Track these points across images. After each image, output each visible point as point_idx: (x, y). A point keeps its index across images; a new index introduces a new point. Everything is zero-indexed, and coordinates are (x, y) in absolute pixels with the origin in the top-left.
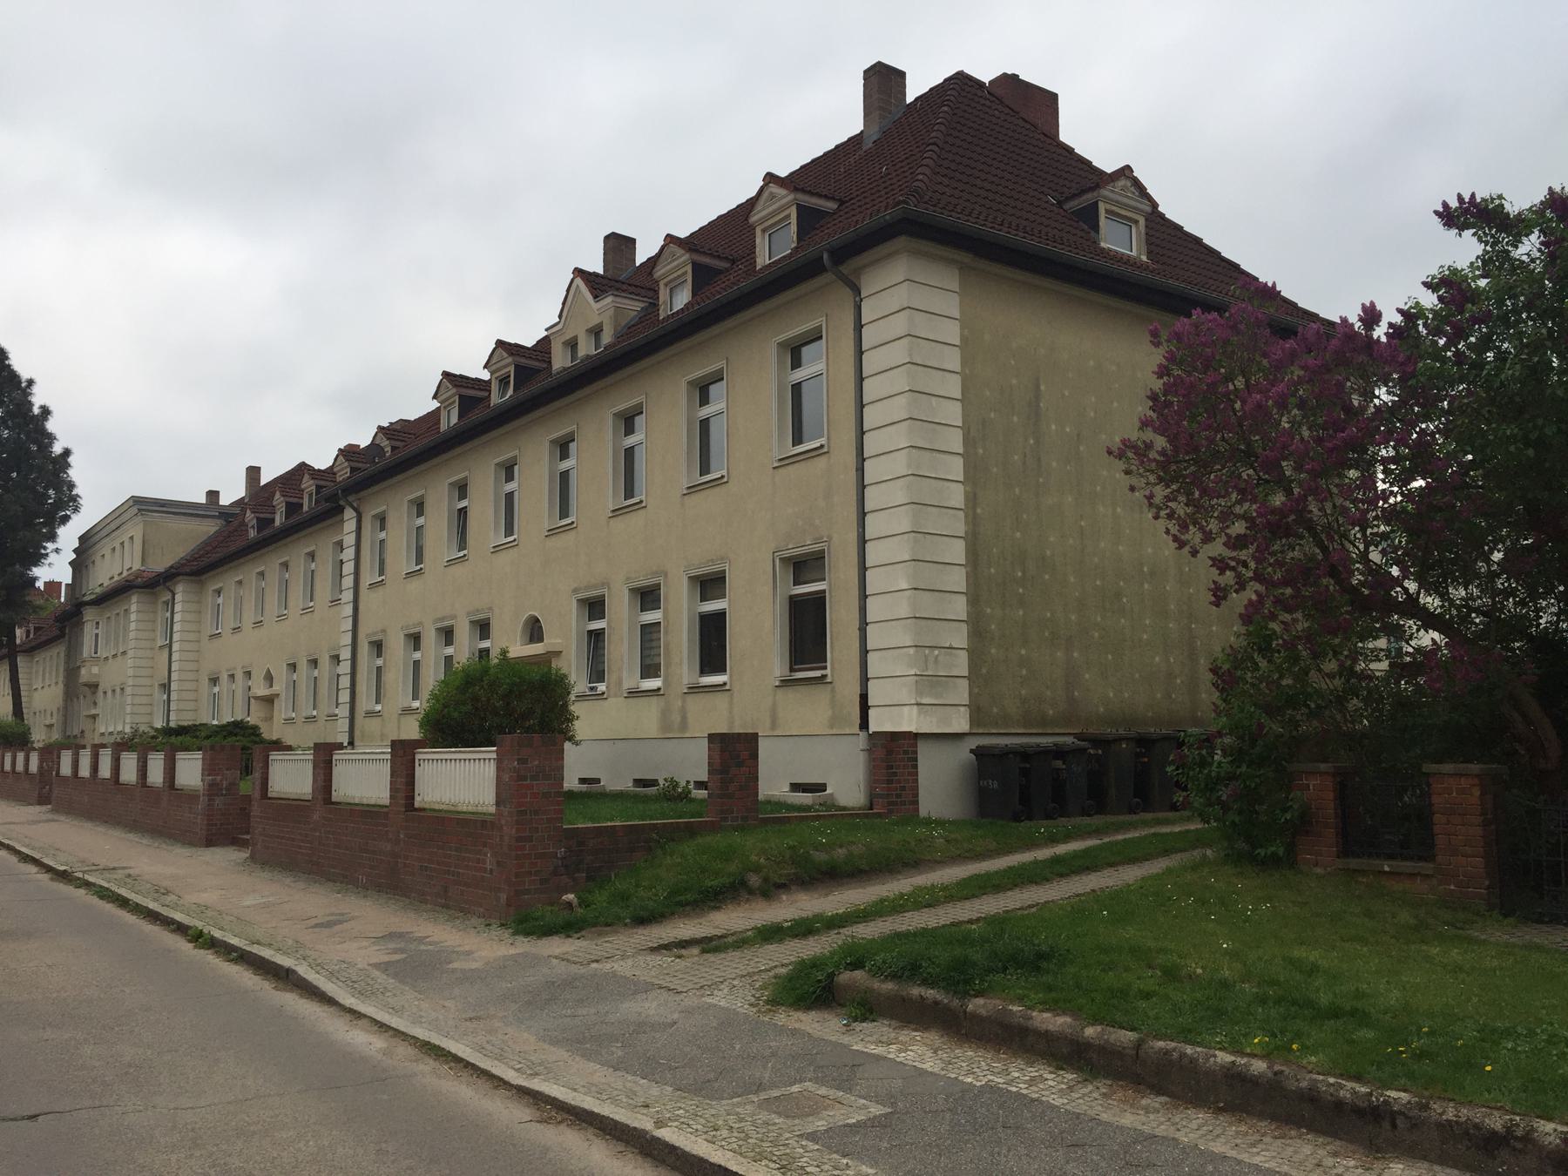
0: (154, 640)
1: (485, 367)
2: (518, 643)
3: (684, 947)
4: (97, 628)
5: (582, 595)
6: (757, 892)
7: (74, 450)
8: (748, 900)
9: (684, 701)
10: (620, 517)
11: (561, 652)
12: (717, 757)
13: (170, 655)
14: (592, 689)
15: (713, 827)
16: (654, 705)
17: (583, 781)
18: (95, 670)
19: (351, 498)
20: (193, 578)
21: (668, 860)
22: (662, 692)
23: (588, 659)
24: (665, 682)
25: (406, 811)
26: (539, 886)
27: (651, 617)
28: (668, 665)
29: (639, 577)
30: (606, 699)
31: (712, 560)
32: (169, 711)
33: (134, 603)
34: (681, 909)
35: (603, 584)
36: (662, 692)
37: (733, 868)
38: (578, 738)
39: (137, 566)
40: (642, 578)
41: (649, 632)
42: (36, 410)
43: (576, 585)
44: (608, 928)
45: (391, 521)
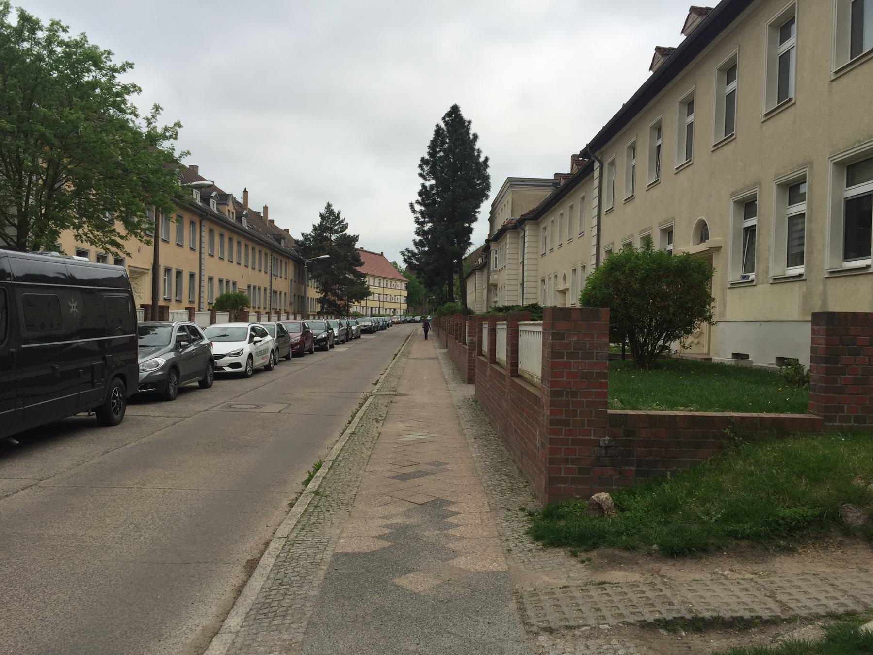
0: (518, 259)
1: (682, 32)
2: (691, 243)
3: (698, 630)
4: (496, 254)
5: (737, 198)
6: (858, 534)
7: (490, 157)
8: (841, 545)
9: (825, 286)
10: (772, 120)
11: (721, 247)
12: (823, 342)
13: (523, 267)
14: (744, 277)
15: (812, 428)
16: (796, 291)
17: (736, 356)
18: (496, 277)
19: (596, 154)
20: (532, 221)
21: (739, 465)
22: (804, 278)
23: (744, 253)
24: (807, 269)
25: (511, 376)
26: (577, 476)
27: (799, 208)
28: (811, 252)
29: (787, 171)
30: (755, 285)
31: (859, 141)
32: (523, 299)
33: (509, 238)
34: (735, 542)
35: (755, 184)
36: (804, 278)
37: (822, 493)
38: (714, 319)
39: (510, 217)
40: (789, 173)
41: (796, 223)
42: (471, 137)
43: (733, 190)
44: (626, 554)
45: (617, 164)
